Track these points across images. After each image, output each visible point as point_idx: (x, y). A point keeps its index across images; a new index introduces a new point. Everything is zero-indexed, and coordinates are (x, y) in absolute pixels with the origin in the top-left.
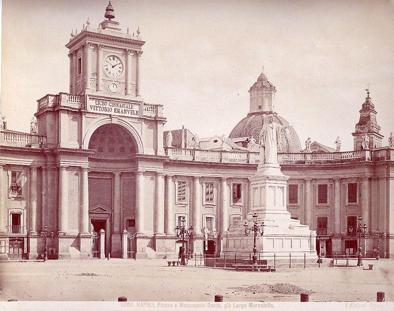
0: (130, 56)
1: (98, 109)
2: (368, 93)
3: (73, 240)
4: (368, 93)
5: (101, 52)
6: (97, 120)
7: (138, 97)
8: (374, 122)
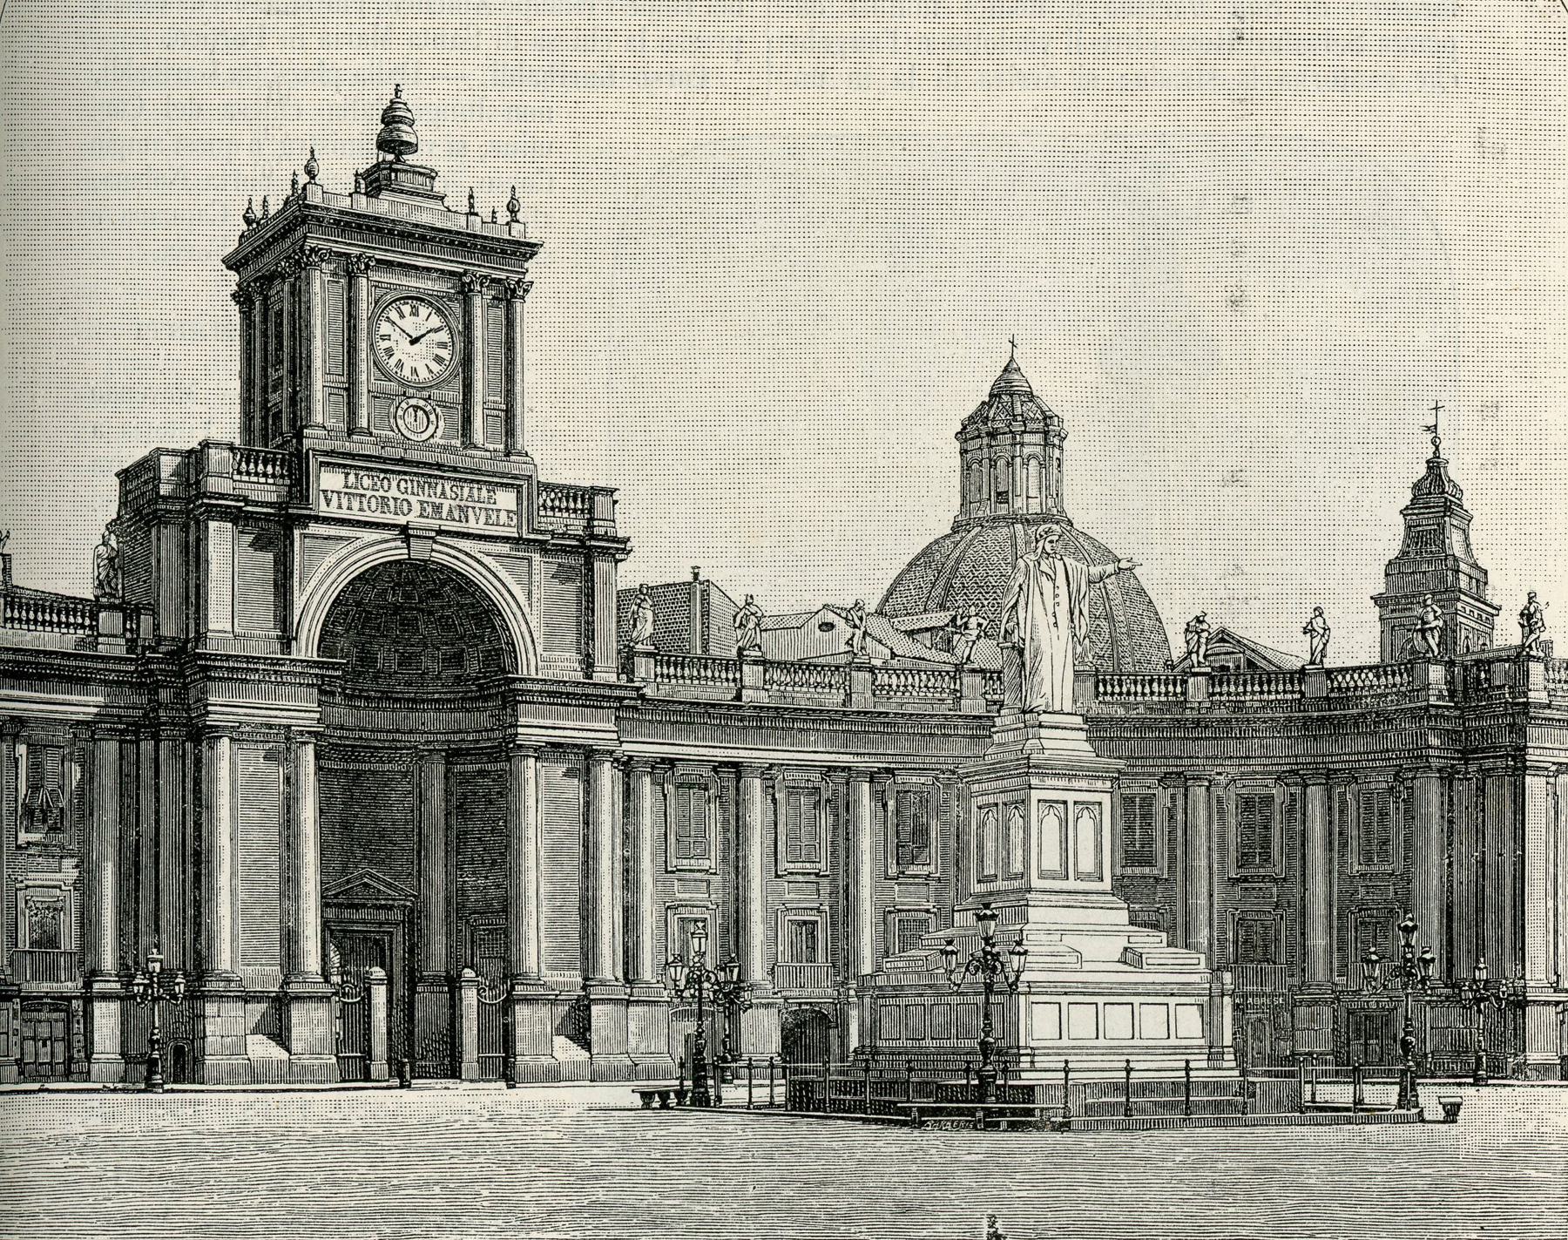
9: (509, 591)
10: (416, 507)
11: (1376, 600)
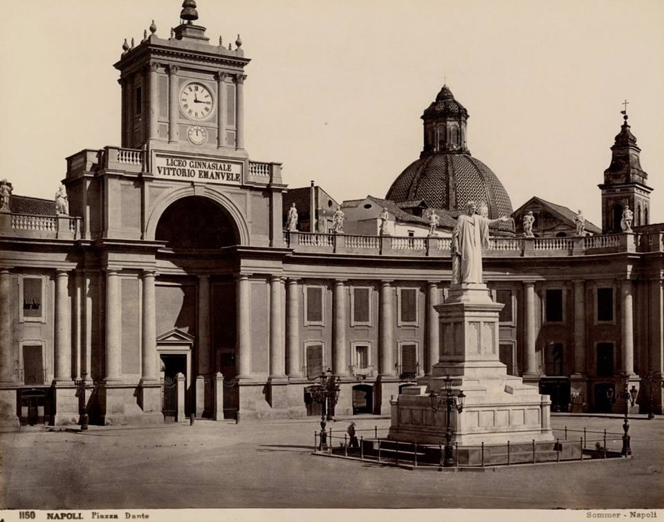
0: (226, 83)
1: (171, 172)
2: (626, 117)
3: (96, 153)
4: (626, 117)
5: (175, 78)
6: (170, 190)
7: (238, 151)
8: (636, 166)
9: (236, 207)
10: (197, 173)
11: (601, 186)
